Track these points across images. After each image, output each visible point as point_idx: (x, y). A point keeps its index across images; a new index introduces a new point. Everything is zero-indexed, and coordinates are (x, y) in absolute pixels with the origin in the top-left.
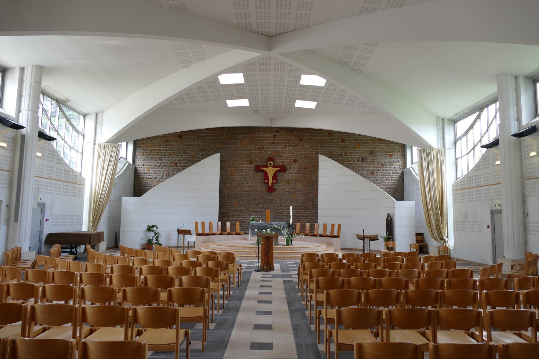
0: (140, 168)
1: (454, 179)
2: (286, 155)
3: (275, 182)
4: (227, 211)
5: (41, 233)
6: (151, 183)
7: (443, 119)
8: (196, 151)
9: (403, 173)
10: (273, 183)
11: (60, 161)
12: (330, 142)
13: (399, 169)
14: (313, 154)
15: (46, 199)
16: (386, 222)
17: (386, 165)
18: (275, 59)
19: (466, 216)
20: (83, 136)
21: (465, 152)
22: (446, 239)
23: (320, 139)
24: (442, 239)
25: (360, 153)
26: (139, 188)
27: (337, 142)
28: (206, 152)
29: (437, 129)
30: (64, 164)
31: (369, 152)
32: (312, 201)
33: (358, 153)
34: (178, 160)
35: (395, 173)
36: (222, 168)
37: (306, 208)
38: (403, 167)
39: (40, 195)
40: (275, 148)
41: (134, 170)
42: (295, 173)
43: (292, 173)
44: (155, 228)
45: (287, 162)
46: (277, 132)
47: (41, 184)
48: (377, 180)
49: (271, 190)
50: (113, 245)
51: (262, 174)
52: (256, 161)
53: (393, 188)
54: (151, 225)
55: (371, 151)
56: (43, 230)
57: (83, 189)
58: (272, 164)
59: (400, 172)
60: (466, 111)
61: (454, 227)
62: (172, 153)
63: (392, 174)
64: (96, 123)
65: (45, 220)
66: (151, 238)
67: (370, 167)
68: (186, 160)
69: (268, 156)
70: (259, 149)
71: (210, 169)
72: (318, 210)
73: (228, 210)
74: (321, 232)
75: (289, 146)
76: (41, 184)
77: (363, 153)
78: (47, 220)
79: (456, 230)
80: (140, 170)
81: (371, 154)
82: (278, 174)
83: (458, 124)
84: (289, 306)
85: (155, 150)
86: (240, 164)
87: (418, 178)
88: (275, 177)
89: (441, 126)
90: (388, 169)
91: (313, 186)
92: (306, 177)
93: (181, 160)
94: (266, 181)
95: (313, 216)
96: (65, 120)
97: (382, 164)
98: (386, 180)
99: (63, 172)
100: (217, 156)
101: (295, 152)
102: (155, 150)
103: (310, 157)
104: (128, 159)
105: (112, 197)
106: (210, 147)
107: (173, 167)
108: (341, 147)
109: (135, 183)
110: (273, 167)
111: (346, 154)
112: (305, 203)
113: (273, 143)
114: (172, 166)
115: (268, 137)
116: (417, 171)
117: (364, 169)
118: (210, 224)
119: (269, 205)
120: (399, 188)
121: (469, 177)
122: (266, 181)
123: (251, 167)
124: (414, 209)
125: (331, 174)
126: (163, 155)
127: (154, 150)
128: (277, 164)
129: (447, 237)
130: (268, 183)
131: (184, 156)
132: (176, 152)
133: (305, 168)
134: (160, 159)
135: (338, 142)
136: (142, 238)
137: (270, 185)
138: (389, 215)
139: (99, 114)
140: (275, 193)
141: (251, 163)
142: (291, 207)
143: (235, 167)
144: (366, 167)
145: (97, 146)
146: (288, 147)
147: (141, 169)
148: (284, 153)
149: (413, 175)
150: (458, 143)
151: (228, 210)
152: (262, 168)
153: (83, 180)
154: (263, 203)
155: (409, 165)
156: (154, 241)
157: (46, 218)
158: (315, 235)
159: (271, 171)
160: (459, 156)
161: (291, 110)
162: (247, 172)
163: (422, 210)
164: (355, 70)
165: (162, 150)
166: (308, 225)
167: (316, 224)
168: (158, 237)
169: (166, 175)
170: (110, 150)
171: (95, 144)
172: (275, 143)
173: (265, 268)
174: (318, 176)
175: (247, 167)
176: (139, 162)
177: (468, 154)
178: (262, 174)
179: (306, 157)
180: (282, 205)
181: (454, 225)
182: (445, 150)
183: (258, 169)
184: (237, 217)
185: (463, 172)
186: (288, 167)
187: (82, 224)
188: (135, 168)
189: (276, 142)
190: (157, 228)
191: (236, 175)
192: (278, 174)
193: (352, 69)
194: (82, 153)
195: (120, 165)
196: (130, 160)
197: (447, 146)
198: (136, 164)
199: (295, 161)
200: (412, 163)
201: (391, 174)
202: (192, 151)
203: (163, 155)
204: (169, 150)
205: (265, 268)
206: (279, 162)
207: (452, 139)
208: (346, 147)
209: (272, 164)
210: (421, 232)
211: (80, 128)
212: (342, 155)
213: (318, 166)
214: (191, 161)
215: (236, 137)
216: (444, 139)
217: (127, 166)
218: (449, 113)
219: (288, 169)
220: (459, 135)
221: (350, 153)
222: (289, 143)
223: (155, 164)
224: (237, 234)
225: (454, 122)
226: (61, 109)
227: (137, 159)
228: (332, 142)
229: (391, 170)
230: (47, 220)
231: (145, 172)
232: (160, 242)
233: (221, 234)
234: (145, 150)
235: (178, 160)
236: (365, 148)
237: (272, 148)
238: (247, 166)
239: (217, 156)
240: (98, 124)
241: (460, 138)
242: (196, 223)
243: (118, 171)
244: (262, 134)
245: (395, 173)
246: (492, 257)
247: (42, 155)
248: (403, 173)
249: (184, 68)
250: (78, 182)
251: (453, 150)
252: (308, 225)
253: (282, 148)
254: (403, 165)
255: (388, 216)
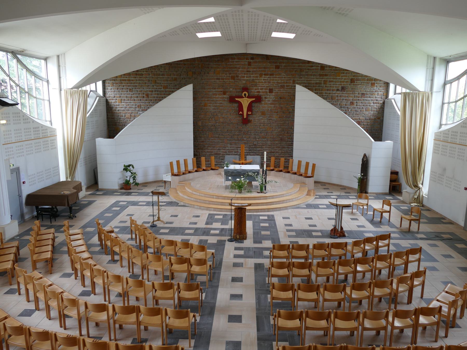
0: (111, 99)
1: (438, 125)
2: (262, 85)
3: (250, 113)
4: (202, 143)
5: (20, 196)
6: (124, 115)
7: (435, 58)
8: (167, 81)
9: (384, 103)
10: (247, 114)
11: (27, 119)
12: (308, 69)
13: (380, 99)
14: (290, 83)
15: (19, 162)
16: (361, 163)
17: (367, 94)
18: (249, 12)
19: (445, 170)
20: (48, 82)
21: (453, 99)
22: (421, 186)
23: (298, 66)
24: (416, 186)
25: (341, 82)
26: (112, 125)
27: (316, 69)
28: (178, 82)
29: (427, 69)
30: (31, 122)
31: (350, 81)
32: (287, 133)
33: (338, 82)
34: (150, 91)
35: (376, 103)
36: (195, 99)
37: (281, 140)
38: (384, 97)
39: (12, 162)
40: (250, 77)
41: (105, 102)
42: (271, 104)
43: (268, 103)
44: (131, 167)
45: (263, 92)
46: (252, 59)
47: (11, 149)
48: (356, 111)
49: (246, 121)
50: (93, 182)
51: (236, 105)
52: (230, 92)
53: (372, 119)
54: (126, 164)
55: (352, 79)
56: (21, 193)
57: (55, 140)
58: (247, 95)
59: (382, 102)
60: (462, 55)
61: (431, 177)
62: (143, 83)
63: (372, 104)
64: (59, 66)
65: (22, 183)
66: (128, 179)
67: (350, 96)
68: (157, 91)
69: (242, 86)
70: (233, 78)
71: (182, 101)
72: (293, 141)
73: (202, 142)
74: (295, 169)
75: (265, 75)
76: (11, 149)
77: (344, 82)
78: (24, 183)
79: (432, 179)
80: (112, 101)
81: (351, 82)
82: (253, 104)
83: (451, 65)
84: (258, 330)
85: (125, 80)
86: (214, 94)
87: (399, 113)
88: (250, 108)
89: (432, 66)
90: (369, 99)
91: (289, 117)
92: (281, 108)
93: (152, 91)
94: (241, 113)
95: (288, 148)
96: (25, 70)
97: (363, 94)
98: (366, 111)
99: (32, 130)
100: (190, 87)
101: (271, 81)
102: (125, 80)
103: (287, 86)
104: (98, 91)
105: (86, 138)
106: (182, 77)
107: (145, 99)
108: (320, 75)
109: (107, 115)
110: (248, 97)
111: (325, 82)
112: (281, 135)
113: (247, 71)
114: (144, 97)
115: (243, 65)
116: (399, 105)
117: (343, 99)
118: (185, 161)
119: (244, 136)
120: (379, 118)
121: (452, 132)
122: (241, 113)
123: (225, 98)
124: (391, 150)
125: (307, 105)
126: (133, 86)
127: (123, 80)
128: (252, 94)
129: (422, 184)
130: (243, 115)
131: (155, 87)
132: (147, 82)
133: (281, 98)
134: (131, 90)
135: (318, 69)
136: (120, 179)
137: (245, 117)
138: (365, 155)
139: (60, 57)
140: (249, 124)
141: (224, 93)
142: (265, 153)
143: (208, 98)
144: (346, 97)
145: (63, 92)
146: (263, 76)
147: (113, 101)
148: (259, 82)
149: (394, 108)
150: (448, 86)
151: (202, 142)
152: (236, 99)
153: (54, 131)
154: (238, 135)
155: (391, 95)
156: (132, 181)
157: (22, 181)
158: (289, 172)
159: (245, 102)
160: (446, 101)
161: (267, 38)
162: (221, 103)
163: (400, 156)
164: (340, 13)
165: (133, 81)
166: (282, 160)
167: (291, 160)
168: (135, 177)
169: (138, 107)
170: (77, 96)
171: (61, 90)
172: (250, 71)
173: (238, 237)
174: (294, 107)
175: (220, 98)
176: (110, 94)
177: (456, 102)
178: (236, 105)
179: (282, 87)
180: (257, 137)
181: (431, 174)
182: (432, 93)
183: (232, 100)
184: (212, 149)
185: (450, 122)
186: (264, 97)
187: (59, 175)
188: (107, 100)
189: (251, 70)
190: (133, 167)
191: (210, 106)
192: (253, 104)
193: (337, 13)
194: (49, 101)
195: (90, 101)
196: (100, 92)
197: (435, 89)
198: (107, 95)
199: (271, 91)
200: (395, 93)
201: (370, 107)
202: (164, 81)
203: (133, 86)
204: (139, 80)
205: (238, 237)
206: (254, 92)
207: (442, 82)
208: (326, 75)
209: (247, 95)
210: (397, 170)
211: (43, 75)
212: (320, 83)
213: (294, 96)
214: (163, 91)
215: (209, 65)
216: (432, 80)
217: (98, 101)
218: (443, 51)
219: (264, 99)
220: (449, 78)
221: (330, 82)
222: (265, 71)
223: (126, 95)
224: (212, 169)
225: (447, 61)
226: (19, 61)
227: (107, 91)
228: (310, 70)
229: (372, 100)
230: (24, 183)
231: (117, 104)
232: (137, 181)
233: (196, 171)
234: (115, 80)
235: (150, 91)
236: (346, 76)
237: (247, 77)
238: (221, 96)
239: (190, 87)
240: (61, 68)
241: (451, 82)
242: (171, 164)
243: (88, 108)
244: (236, 62)
245: (376, 103)
246: (464, 218)
247: (7, 121)
248: (384, 103)
249: (145, 14)
250: (49, 134)
251: (441, 94)
252: (282, 160)
253: (257, 77)
254: (385, 94)
255: (364, 157)
